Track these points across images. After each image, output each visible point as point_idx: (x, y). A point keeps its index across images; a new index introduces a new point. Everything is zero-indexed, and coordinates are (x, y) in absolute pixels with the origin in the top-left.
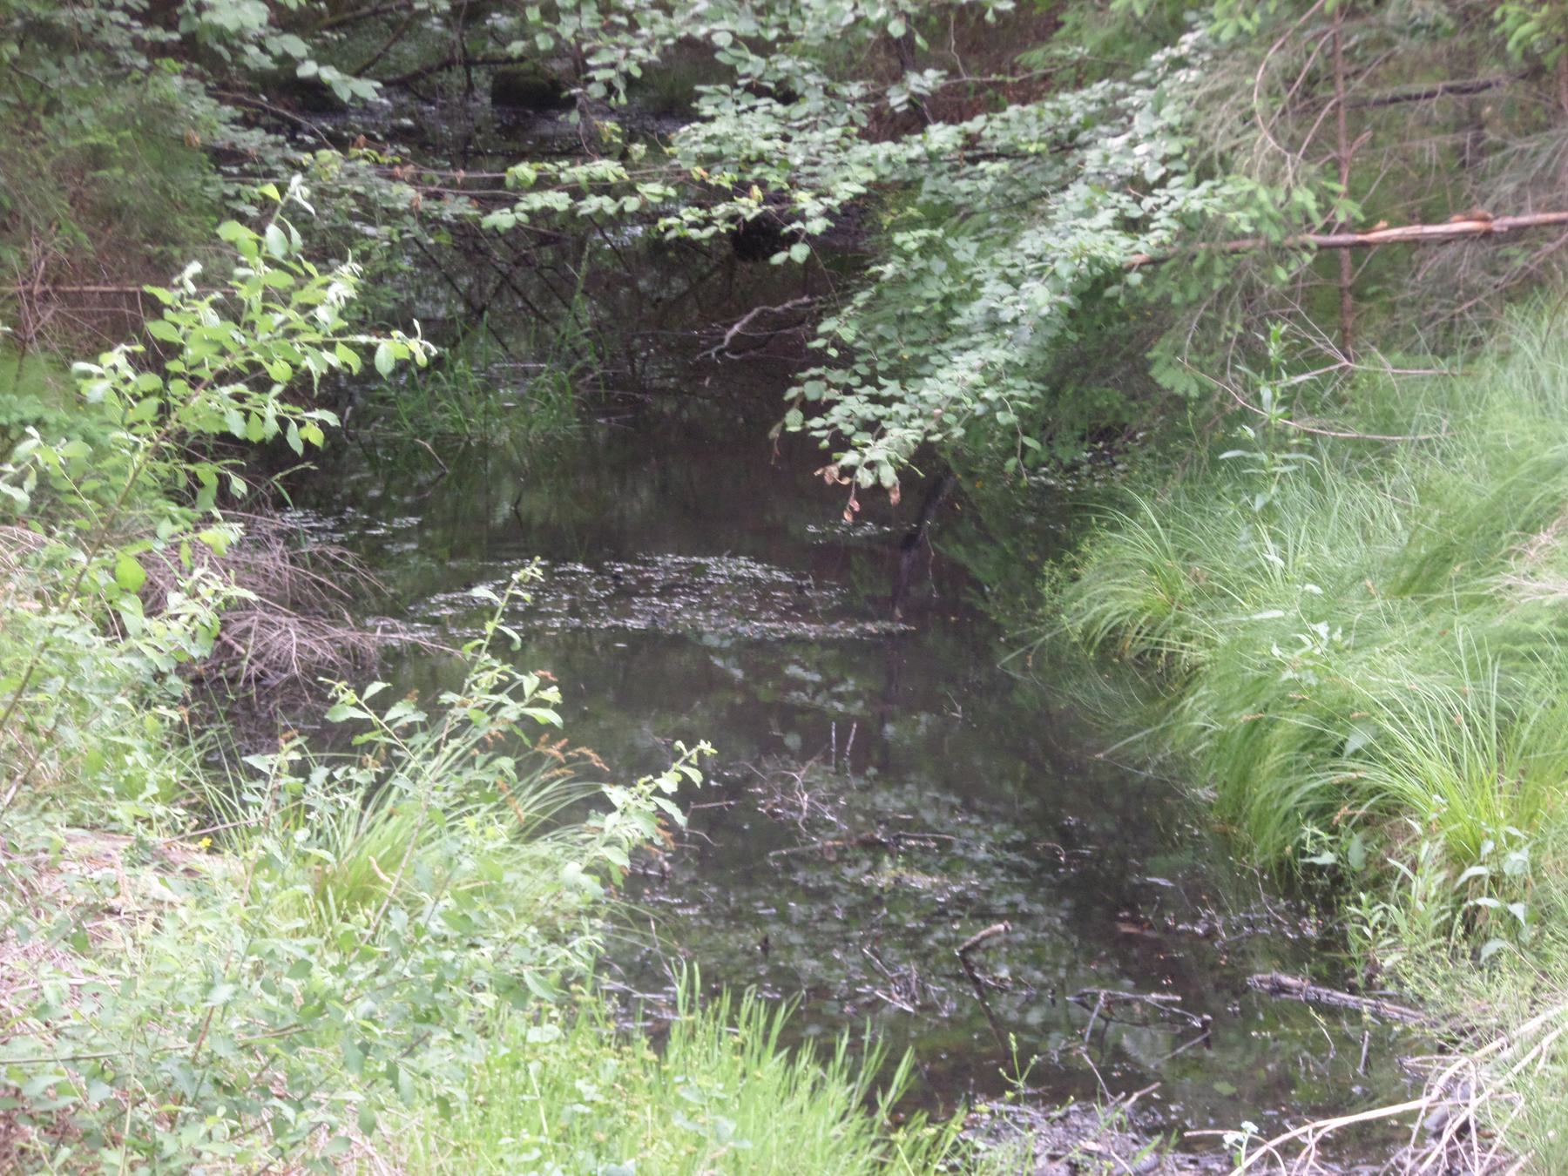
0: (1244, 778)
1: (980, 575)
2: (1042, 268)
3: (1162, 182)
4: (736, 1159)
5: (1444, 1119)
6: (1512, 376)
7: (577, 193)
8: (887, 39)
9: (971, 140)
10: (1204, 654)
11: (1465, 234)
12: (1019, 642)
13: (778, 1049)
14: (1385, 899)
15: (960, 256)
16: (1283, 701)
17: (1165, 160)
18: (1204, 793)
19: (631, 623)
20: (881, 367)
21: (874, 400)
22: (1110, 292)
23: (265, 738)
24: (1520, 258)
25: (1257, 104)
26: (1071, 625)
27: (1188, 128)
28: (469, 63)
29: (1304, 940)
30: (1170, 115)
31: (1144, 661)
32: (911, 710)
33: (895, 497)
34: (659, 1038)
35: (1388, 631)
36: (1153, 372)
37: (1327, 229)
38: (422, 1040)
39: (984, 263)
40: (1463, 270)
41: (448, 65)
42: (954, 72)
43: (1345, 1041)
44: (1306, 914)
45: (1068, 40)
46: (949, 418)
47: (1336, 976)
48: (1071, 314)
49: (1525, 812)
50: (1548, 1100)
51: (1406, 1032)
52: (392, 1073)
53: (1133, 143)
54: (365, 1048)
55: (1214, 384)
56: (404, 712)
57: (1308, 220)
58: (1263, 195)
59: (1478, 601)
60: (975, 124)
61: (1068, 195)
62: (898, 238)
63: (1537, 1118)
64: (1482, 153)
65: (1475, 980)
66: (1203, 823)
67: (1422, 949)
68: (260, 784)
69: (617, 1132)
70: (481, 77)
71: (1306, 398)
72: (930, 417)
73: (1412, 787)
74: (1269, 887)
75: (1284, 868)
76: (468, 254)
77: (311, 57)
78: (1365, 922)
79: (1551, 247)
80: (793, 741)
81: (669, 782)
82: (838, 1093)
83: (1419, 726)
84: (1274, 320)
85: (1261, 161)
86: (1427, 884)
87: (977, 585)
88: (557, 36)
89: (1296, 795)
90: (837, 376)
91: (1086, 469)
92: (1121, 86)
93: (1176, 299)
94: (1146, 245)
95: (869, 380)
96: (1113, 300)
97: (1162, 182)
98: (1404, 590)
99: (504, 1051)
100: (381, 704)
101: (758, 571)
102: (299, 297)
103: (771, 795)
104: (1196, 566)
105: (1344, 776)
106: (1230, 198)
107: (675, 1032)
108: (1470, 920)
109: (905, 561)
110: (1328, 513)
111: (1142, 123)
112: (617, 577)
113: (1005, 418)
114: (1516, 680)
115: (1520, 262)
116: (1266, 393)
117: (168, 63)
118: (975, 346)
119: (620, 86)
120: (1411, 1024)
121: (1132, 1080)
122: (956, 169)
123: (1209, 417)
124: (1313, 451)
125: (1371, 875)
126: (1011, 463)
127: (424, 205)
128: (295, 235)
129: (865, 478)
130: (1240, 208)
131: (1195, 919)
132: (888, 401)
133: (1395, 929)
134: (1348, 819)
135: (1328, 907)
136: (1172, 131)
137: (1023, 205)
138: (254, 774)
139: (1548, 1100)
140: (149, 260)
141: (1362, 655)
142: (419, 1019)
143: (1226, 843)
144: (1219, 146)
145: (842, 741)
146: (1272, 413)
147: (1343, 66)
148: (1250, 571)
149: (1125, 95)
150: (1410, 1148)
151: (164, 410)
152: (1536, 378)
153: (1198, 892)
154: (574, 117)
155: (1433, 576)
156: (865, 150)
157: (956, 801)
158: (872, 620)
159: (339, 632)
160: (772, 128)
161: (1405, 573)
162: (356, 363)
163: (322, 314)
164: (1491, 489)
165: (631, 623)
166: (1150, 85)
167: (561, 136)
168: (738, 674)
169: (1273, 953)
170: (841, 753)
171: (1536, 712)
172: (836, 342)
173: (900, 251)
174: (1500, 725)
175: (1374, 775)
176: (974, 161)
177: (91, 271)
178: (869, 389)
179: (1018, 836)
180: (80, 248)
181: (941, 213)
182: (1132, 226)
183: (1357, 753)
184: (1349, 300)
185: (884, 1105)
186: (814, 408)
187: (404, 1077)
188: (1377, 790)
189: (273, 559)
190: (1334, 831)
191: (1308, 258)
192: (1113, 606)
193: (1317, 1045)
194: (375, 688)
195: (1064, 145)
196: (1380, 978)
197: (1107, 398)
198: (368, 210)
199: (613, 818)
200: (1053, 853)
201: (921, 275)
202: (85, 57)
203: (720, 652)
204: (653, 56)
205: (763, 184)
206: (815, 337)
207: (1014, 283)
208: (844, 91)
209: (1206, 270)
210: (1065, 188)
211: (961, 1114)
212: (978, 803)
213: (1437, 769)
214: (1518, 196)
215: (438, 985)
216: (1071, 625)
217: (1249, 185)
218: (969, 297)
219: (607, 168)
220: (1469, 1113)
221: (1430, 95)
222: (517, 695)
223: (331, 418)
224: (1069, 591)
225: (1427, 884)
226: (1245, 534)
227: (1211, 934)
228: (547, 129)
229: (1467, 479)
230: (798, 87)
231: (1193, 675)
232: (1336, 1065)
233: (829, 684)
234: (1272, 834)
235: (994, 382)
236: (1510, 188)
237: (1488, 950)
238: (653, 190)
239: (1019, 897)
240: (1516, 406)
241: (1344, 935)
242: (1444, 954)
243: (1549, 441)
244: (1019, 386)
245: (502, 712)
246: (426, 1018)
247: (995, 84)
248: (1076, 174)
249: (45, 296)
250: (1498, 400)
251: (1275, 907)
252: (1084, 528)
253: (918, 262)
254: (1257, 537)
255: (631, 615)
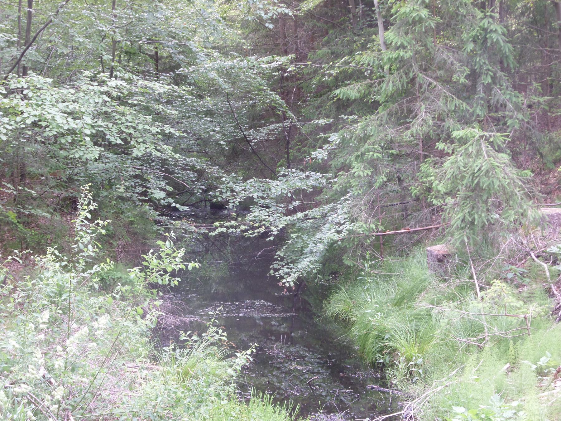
0: (364, 344)
1: (311, 303)
2: (321, 241)
3: (344, 223)
5: (407, 415)
6: (415, 261)
7: (227, 227)
10: (356, 319)
11: (404, 232)
16: (371, 329)
17: (345, 219)
18: (357, 348)
19: (240, 315)
21: (288, 268)
22: (335, 245)
24: (416, 237)
25: (362, 207)
26: (329, 313)
27: (349, 213)
28: (205, 201)
29: (378, 378)
30: (345, 210)
31: (344, 320)
33: (294, 288)
34: (247, 401)
35: (392, 314)
36: (344, 261)
37: (377, 232)
38: (200, 406)
40: (404, 240)
41: (201, 201)
43: (386, 399)
44: (377, 372)
46: (303, 272)
47: (384, 385)
48: (327, 250)
49: (421, 351)
50: (428, 411)
51: (399, 397)
52: (194, 413)
53: (338, 215)
54: (188, 408)
55: (356, 263)
57: (373, 230)
58: (364, 226)
59: (410, 307)
60: (307, 212)
61: (325, 226)
62: (292, 235)
64: (408, 216)
70: (208, 203)
71: (374, 266)
72: (300, 271)
73: (398, 346)
74: (370, 367)
75: (373, 362)
76: (206, 239)
77: (174, 202)
78: (389, 374)
79: (422, 235)
81: (249, 352)
82: (284, 413)
85: (364, 219)
86: (402, 366)
87: (310, 304)
89: (375, 348)
90: (281, 263)
93: (348, 246)
94: (341, 236)
97: (344, 223)
98: (395, 305)
99: (216, 406)
100: (190, 336)
101: (265, 303)
102: (173, 255)
104: (353, 300)
105: (385, 344)
106: (358, 226)
107: (251, 401)
108: (411, 373)
109: (295, 299)
110: (379, 289)
111: (340, 212)
112: (237, 305)
115: (416, 238)
116: (366, 265)
117: (145, 204)
118: (308, 257)
122: (303, 221)
123: (355, 270)
124: (376, 277)
125: (390, 364)
126: (316, 281)
127: (197, 230)
128: (172, 243)
130: (360, 228)
131: (355, 374)
132: (291, 269)
133: (396, 375)
135: (382, 371)
136: (346, 213)
138: (165, 351)
140: (142, 243)
143: (362, 358)
144: (355, 216)
145: (283, 338)
146: (367, 269)
147: (379, 199)
148: (364, 301)
151: (146, 278)
153: (356, 368)
154: (226, 212)
155: (401, 302)
156: (285, 218)
157: (307, 349)
158: (289, 313)
159: (181, 318)
160: (266, 214)
161: (395, 302)
162: (184, 268)
164: (412, 284)
165: (240, 315)
167: (224, 215)
168: (262, 324)
169: (371, 381)
170: (283, 341)
171: (423, 330)
172: (280, 256)
173: (292, 238)
175: (391, 344)
176: (306, 219)
178: (287, 266)
179: (320, 356)
180: (128, 241)
181: (300, 230)
182: (338, 232)
183: (387, 339)
184: (382, 246)
186: (277, 270)
187: (196, 414)
188: (391, 347)
189: (168, 304)
190: (383, 355)
191: (374, 238)
192: (337, 309)
193: (381, 400)
194: (189, 332)
195: (324, 216)
196: (393, 386)
197: (334, 266)
198: (186, 231)
199: (238, 359)
202: (129, 202)
205: (264, 225)
213: (403, 342)
215: (203, 395)
216: (329, 313)
217: (361, 224)
219: (233, 223)
220: (412, 414)
221: (397, 204)
223: (179, 280)
224: (328, 306)
225: (402, 366)
226: (363, 294)
229: (407, 282)
230: (270, 206)
231: (354, 323)
233: (280, 325)
234: (371, 356)
235: (312, 264)
236: (413, 223)
237: (415, 379)
238: (243, 227)
239: (320, 369)
241: (385, 377)
243: (423, 274)
244: (317, 265)
245: (215, 338)
246: (201, 402)
249: (121, 252)
250: (413, 266)
251: (370, 371)
253: (296, 240)
254: (365, 295)
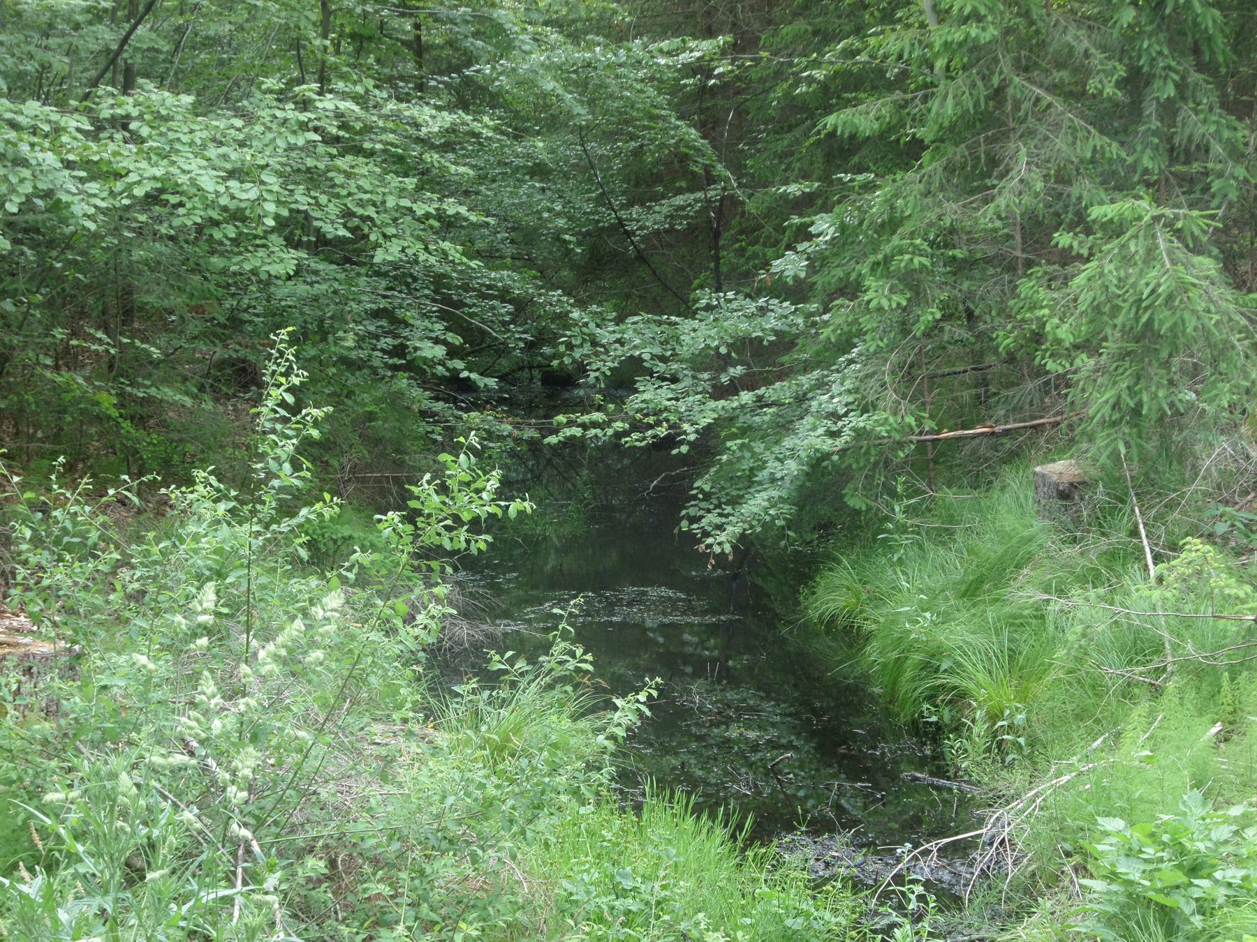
0: (895, 683)
3: (846, 414)
4: (676, 866)
5: (993, 836)
7: (584, 427)
8: (718, 354)
9: (760, 398)
10: (874, 627)
11: (982, 434)
12: (791, 623)
13: (692, 814)
14: (960, 736)
15: (757, 450)
16: (911, 648)
17: (846, 405)
18: (877, 690)
19: (614, 619)
20: (723, 500)
21: (720, 515)
22: (825, 464)
23: (458, 676)
24: (1008, 444)
25: (887, 378)
26: (813, 614)
27: (857, 390)
29: (925, 756)
30: (848, 384)
31: (848, 630)
32: (741, 654)
33: (730, 558)
34: (638, 808)
35: (957, 615)
37: (921, 433)
38: (536, 816)
39: (768, 453)
40: (982, 450)
41: (522, 369)
42: (749, 367)
43: (945, 802)
44: (925, 744)
45: (800, 351)
46: (754, 523)
47: (940, 772)
48: (807, 474)
49: (1022, 695)
52: (523, 833)
53: (832, 397)
55: (873, 504)
56: (521, 665)
58: (891, 420)
60: (760, 392)
61: (804, 421)
62: (729, 444)
63: (1036, 836)
65: (1004, 773)
66: (877, 703)
67: (979, 759)
68: (459, 699)
69: (620, 854)
70: (536, 373)
73: (971, 685)
74: (908, 733)
77: (466, 369)
78: (952, 747)
79: (1021, 439)
80: (689, 670)
81: (642, 697)
82: (720, 833)
83: (973, 658)
84: (899, 475)
86: (980, 729)
87: (768, 596)
88: (573, 358)
89: (919, 691)
90: (704, 505)
91: (816, 542)
92: (826, 372)
93: (854, 466)
94: (840, 443)
95: (718, 506)
96: (826, 468)
97: (846, 414)
98: (963, 596)
103: (681, 696)
104: (868, 587)
105: (940, 682)
106: (876, 421)
109: (734, 585)
110: (927, 561)
111: (835, 388)
112: (607, 598)
113: (779, 523)
114: (1016, 636)
115: (1008, 446)
116: (897, 508)
117: (400, 374)
118: (765, 490)
119: (601, 377)
120: (976, 793)
121: (851, 823)
122: (752, 411)
123: (871, 519)
124: (918, 534)
126: (783, 543)
129: (717, 549)
132: (727, 516)
134: (943, 701)
136: (849, 392)
137: (783, 426)
138: (457, 695)
139: (1040, 827)
140: (394, 462)
141: (946, 626)
142: (535, 808)
143: (888, 713)
144: (870, 399)
145: (713, 670)
146: (900, 517)
149: (827, 376)
150: (979, 851)
152: (1018, 498)
153: (876, 735)
155: (976, 589)
158: (724, 614)
159: (485, 627)
161: (963, 588)
163: (484, 495)
164: (1000, 549)
165: (614, 619)
166: (838, 371)
168: (661, 640)
169: (910, 762)
170: (712, 676)
171: (1025, 650)
172: (701, 490)
174: (1010, 656)
175: (954, 681)
176: (761, 407)
177: (369, 467)
178: (718, 510)
182: (834, 435)
183: (945, 671)
184: (931, 465)
185: (740, 838)
186: (694, 520)
187: (529, 834)
188: (955, 688)
190: (936, 706)
191: (913, 447)
192: (832, 605)
193: (933, 804)
194: (510, 653)
197: (824, 510)
200: (809, 720)
201: (739, 459)
203: (651, 629)
204: (616, 364)
205: (667, 421)
206: (692, 489)
207: (781, 461)
208: (701, 376)
209: (867, 453)
210: (802, 418)
211: (776, 841)
212: (773, 695)
213: (981, 677)
214: (1006, 416)
215: (543, 793)
216: (813, 614)
218: (762, 468)
222: (573, 655)
223: (489, 538)
225: (980, 729)
226: (890, 572)
227: (883, 754)
228: (567, 395)
230: (680, 376)
231: (869, 637)
232: (942, 813)
234: (909, 709)
236: (1002, 412)
237: (1009, 758)
238: (619, 425)
239: (793, 737)
240: (1009, 512)
241: (942, 753)
242: (989, 761)
246: (538, 807)
247: (768, 372)
248: (807, 411)
249: (349, 480)
250: (1002, 509)
251: (909, 742)
252: (817, 570)
253: (738, 454)
254: (895, 573)
255: (614, 615)
